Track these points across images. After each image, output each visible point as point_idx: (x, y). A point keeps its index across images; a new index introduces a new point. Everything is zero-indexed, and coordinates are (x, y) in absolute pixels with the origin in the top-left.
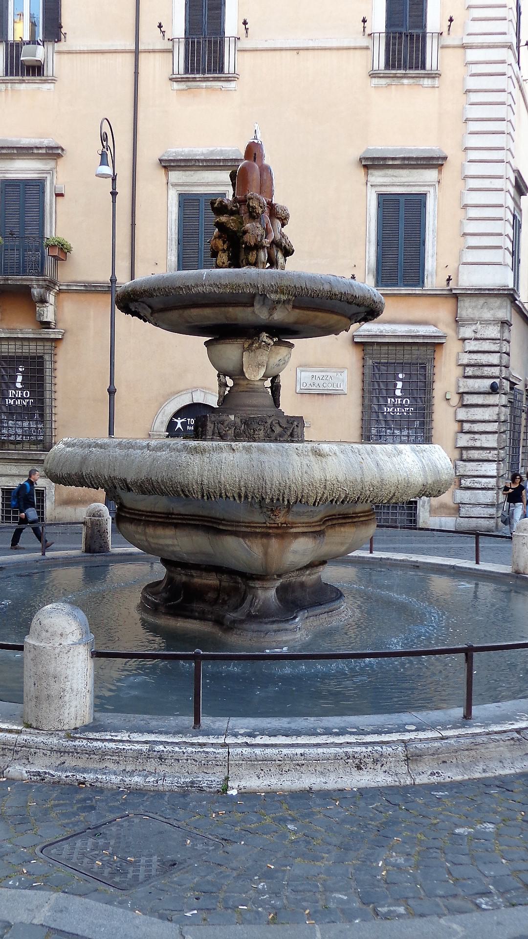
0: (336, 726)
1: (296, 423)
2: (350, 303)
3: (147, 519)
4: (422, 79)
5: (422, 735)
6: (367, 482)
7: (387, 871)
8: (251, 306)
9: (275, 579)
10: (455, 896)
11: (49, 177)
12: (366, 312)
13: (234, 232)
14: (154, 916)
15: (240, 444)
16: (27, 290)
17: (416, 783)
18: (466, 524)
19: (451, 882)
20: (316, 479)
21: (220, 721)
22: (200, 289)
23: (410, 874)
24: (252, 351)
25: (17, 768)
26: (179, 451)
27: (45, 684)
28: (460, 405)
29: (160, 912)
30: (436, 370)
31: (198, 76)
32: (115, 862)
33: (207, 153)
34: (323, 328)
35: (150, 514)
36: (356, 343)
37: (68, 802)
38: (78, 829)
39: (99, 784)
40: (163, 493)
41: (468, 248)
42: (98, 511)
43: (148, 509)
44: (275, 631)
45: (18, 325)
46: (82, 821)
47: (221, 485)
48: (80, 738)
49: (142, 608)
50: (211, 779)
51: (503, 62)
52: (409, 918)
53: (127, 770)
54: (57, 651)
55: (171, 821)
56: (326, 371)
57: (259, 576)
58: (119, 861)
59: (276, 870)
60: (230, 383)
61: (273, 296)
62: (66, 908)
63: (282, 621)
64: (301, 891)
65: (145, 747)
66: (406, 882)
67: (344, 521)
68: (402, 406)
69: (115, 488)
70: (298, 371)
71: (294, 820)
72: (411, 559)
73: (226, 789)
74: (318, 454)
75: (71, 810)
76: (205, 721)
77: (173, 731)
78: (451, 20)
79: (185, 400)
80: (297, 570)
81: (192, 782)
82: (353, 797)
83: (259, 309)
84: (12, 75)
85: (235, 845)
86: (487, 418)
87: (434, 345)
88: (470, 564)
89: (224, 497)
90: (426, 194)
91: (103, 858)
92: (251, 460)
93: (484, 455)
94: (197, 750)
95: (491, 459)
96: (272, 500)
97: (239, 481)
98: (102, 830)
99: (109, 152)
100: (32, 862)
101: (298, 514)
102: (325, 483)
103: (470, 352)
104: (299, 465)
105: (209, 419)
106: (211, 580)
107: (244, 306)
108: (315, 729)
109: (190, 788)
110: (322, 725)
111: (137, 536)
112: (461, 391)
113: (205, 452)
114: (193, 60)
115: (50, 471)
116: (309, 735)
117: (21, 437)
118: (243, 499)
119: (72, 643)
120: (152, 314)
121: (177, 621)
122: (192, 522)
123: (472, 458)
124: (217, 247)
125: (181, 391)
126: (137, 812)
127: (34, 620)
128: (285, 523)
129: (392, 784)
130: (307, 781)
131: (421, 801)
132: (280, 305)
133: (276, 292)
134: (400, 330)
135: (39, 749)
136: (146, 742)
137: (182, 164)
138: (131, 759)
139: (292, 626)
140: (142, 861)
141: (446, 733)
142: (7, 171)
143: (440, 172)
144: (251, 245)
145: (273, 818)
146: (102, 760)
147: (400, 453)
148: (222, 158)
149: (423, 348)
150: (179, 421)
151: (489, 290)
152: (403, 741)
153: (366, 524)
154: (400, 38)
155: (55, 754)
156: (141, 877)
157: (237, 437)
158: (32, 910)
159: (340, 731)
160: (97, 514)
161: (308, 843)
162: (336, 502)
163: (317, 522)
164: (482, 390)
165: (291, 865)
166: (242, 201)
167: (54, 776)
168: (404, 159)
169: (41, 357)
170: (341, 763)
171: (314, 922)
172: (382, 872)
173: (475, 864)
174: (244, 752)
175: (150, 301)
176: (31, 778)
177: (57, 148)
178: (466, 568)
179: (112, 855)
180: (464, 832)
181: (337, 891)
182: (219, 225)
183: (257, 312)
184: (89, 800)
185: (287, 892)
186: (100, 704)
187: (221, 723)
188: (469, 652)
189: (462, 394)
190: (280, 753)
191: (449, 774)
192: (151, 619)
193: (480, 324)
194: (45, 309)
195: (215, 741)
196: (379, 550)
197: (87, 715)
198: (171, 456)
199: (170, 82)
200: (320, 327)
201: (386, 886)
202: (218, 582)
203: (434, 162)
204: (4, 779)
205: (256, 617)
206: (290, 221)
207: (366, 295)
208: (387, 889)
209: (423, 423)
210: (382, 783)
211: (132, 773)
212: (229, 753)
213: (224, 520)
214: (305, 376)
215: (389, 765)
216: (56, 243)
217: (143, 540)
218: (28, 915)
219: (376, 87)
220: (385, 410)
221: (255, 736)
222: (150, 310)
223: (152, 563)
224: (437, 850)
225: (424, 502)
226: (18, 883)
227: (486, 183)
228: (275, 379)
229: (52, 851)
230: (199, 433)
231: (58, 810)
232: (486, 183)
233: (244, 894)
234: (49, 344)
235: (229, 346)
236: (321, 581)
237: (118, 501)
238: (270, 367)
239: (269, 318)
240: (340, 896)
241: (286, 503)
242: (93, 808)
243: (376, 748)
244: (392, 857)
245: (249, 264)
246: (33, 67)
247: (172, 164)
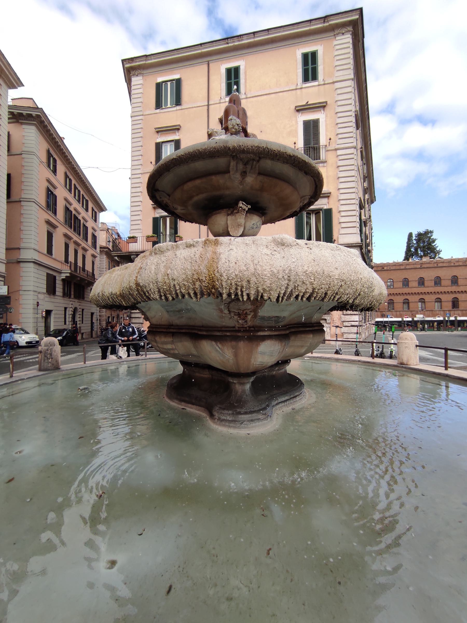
12: (310, 195)
78: (330, 139)
151: (352, 244)
154: (310, 149)
162: (302, 299)
202: (210, 376)
227: (348, 202)
232: (348, 202)
238: (247, 229)
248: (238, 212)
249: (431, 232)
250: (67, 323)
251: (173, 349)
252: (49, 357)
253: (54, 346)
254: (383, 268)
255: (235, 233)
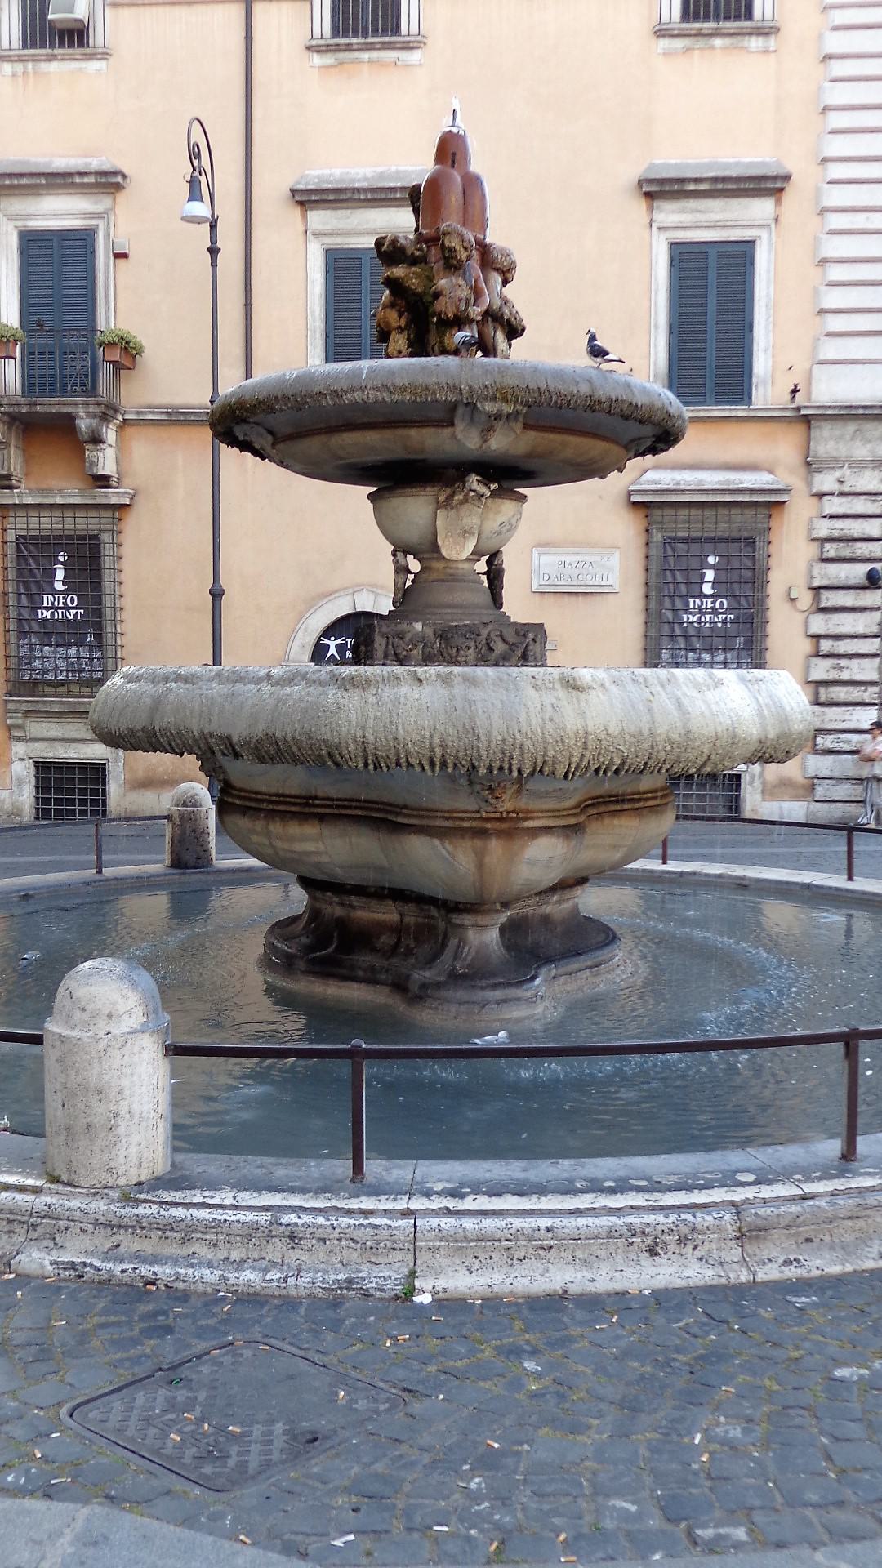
0: (610, 1175)
1: (531, 635)
2: (626, 418)
3: (271, 807)
4: (747, 38)
5: (767, 1192)
6: (660, 735)
7: (711, 1454)
8: (447, 426)
9: (497, 911)
10: (841, 1504)
11: (101, 225)
12: (654, 436)
13: (415, 294)
14: (272, 1550)
15: (432, 670)
16: (70, 418)
17: (758, 1279)
18: (824, 813)
19: (833, 1475)
20: (568, 730)
21: (399, 1167)
22: (357, 396)
23: (753, 1459)
24: (452, 508)
25: (33, 1255)
26: (322, 684)
27: (81, 1105)
28: (814, 608)
29: (287, 1537)
30: (773, 549)
31: (355, 40)
32: (204, 1434)
33: (373, 177)
34: (579, 465)
35: (278, 799)
36: (635, 504)
37: (124, 1318)
38: (140, 1371)
39: (181, 1285)
40: (296, 760)
41: (829, 334)
42: (192, 797)
43: (273, 791)
44: (498, 1002)
45: (55, 483)
46: (148, 1357)
47: (399, 744)
48: (146, 1201)
49: (266, 963)
50: (384, 1275)
52: (755, 1550)
53: (232, 1258)
54: (102, 1045)
55: (311, 1355)
56: (582, 554)
57: (469, 906)
58: (212, 1434)
59: (501, 1453)
60: (415, 566)
61: (489, 407)
62: (106, 1538)
63: (509, 985)
64: (549, 1495)
65: (264, 1218)
66: (747, 1476)
67: (618, 807)
68: (715, 612)
69: (213, 752)
70: (535, 555)
71: (534, 1353)
72: (734, 874)
73: (410, 1292)
74: (572, 685)
75: (130, 1334)
76: (374, 1167)
77: (315, 1186)
79: (342, 608)
80: (537, 894)
81: (350, 1281)
82: (643, 1308)
83: (462, 431)
84: (34, 46)
85: (427, 1402)
86: (861, 630)
87: (770, 505)
88: (837, 881)
89: (404, 764)
90: (753, 242)
91: (185, 1426)
92: (452, 698)
93: (856, 694)
94: (357, 1223)
95: (867, 700)
96: (490, 769)
97: (431, 736)
98: (185, 1372)
99: (203, 179)
100: (54, 1435)
101: (538, 795)
102: (585, 738)
103: (832, 517)
104: (539, 706)
105: (377, 630)
106: (387, 913)
107: (437, 426)
108: (572, 1181)
109: (345, 1291)
110: (584, 1172)
111: (255, 838)
112: (816, 583)
113: (370, 685)
114: (346, 12)
115: (99, 724)
116: (562, 1194)
117: (64, 673)
118: (437, 768)
119: (128, 1030)
120: (273, 445)
121: (328, 985)
122: (349, 812)
123: (835, 699)
124: (388, 324)
125: (336, 591)
126: (247, 1337)
127: (61, 990)
128: (514, 812)
129: (715, 1282)
130: (559, 1277)
131: (767, 1314)
132: (501, 423)
133: (494, 399)
134: (709, 480)
135: (73, 1221)
136: (266, 1209)
137: (331, 197)
138: (238, 1238)
139: (529, 994)
140: (255, 1433)
141: (810, 1188)
142: (30, 216)
143: (778, 202)
144: (448, 318)
145: (496, 1348)
146: (185, 1241)
147: (719, 683)
148: (399, 184)
149: (749, 512)
150: (332, 643)
151: (865, 407)
152: (733, 1203)
153: (657, 812)
155: (102, 1231)
156: (253, 1466)
157: (428, 660)
158: (40, 1543)
159: (617, 1186)
160: (192, 802)
161: (562, 1397)
162: (605, 772)
163: (571, 809)
164: (852, 582)
165: (530, 1442)
166: (430, 239)
167: (99, 1270)
168: (715, 180)
169: (96, 537)
170: (620, 1244)
171: (574, 1558)
172: (702, 1455)
173: (875, 1438)
174: (442, 1225)
175: (271, 420)
176: (59, 1274)
177: (115, 173)
178: (830, 888)
179: (201, 1420)
180: (852, 1375)
181: (620, 1493)
182: (390, 283)
183: (459, 436)
184: (161, 1315)
185: (524, 1496)
186: (184, 1136)
187: (402, 1171)
188: (850, 1040)
189: (817, 590)
190: (508, 1227)
191: (818, 1262)
192: (280, 982)
193: (850, 467)
194: (100, 454)
195: (390, 1206)
196: (676, 858)
197: (160, 1161)
198: (309, 694)
199: (306, 53)
200: (569, 463)
201: (709, 1483)
204: (12, 1276)
205: (464, 977)
206: (518, 276)
207: (656, 403)
208: (711, 1489)
209: (750, 641)
210: (696, 1280)
211: (240, 1265)
212: (415, 1227)
213: (405, 807)
214: (547, 563)
215: (707, 1246)
216: (116, 339)
217: (265, 845)
218: (31, 1552)
219: (667, 54)
220: (685, 620)
221: (462, 1196)
222: (270, 438)
223: (287, 886)
224: (802, 1412)
225: (753, 777)
226: (23, 1479)
228: (494, 558)
229: (91, 1415)
230: (361, 655)
231: (105, 1334)
233: (443, 1500)
234: (109, 514)
235: (410, 499)
236: (578, 912)
237: (221, 777)
238: (484, 537)
239: (481, 447)
240: (625, 1505)
241: (515, 774)
242: (169, 1330)
243: (683, 1216)
244: (718, 1424)
245: (444, 352)
246: (71, 32)
247: (313, 198)
248: (466, 501)
251: (317, 853)
255: (454, 552)
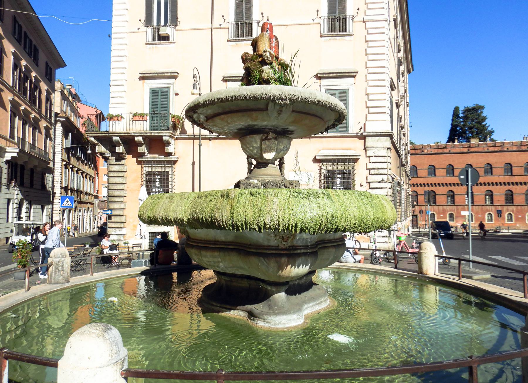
11: (172, 86)
51: (384, 27)
78: (358, 9)
103: (372, 163)
177: (176, 73)
203: (351, 75)
249: (482, 107)
250: (10, 220)
252: (60, 270)
253: (66, 257)
254: (423, 151)
